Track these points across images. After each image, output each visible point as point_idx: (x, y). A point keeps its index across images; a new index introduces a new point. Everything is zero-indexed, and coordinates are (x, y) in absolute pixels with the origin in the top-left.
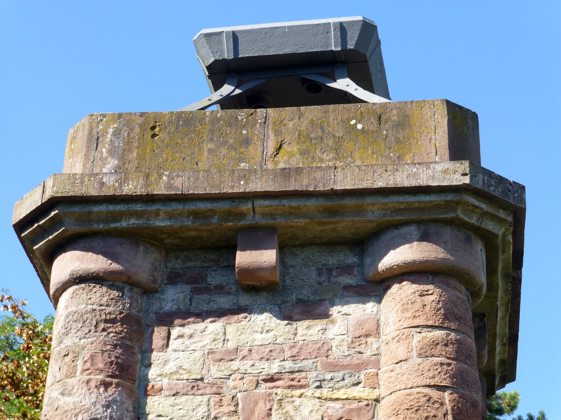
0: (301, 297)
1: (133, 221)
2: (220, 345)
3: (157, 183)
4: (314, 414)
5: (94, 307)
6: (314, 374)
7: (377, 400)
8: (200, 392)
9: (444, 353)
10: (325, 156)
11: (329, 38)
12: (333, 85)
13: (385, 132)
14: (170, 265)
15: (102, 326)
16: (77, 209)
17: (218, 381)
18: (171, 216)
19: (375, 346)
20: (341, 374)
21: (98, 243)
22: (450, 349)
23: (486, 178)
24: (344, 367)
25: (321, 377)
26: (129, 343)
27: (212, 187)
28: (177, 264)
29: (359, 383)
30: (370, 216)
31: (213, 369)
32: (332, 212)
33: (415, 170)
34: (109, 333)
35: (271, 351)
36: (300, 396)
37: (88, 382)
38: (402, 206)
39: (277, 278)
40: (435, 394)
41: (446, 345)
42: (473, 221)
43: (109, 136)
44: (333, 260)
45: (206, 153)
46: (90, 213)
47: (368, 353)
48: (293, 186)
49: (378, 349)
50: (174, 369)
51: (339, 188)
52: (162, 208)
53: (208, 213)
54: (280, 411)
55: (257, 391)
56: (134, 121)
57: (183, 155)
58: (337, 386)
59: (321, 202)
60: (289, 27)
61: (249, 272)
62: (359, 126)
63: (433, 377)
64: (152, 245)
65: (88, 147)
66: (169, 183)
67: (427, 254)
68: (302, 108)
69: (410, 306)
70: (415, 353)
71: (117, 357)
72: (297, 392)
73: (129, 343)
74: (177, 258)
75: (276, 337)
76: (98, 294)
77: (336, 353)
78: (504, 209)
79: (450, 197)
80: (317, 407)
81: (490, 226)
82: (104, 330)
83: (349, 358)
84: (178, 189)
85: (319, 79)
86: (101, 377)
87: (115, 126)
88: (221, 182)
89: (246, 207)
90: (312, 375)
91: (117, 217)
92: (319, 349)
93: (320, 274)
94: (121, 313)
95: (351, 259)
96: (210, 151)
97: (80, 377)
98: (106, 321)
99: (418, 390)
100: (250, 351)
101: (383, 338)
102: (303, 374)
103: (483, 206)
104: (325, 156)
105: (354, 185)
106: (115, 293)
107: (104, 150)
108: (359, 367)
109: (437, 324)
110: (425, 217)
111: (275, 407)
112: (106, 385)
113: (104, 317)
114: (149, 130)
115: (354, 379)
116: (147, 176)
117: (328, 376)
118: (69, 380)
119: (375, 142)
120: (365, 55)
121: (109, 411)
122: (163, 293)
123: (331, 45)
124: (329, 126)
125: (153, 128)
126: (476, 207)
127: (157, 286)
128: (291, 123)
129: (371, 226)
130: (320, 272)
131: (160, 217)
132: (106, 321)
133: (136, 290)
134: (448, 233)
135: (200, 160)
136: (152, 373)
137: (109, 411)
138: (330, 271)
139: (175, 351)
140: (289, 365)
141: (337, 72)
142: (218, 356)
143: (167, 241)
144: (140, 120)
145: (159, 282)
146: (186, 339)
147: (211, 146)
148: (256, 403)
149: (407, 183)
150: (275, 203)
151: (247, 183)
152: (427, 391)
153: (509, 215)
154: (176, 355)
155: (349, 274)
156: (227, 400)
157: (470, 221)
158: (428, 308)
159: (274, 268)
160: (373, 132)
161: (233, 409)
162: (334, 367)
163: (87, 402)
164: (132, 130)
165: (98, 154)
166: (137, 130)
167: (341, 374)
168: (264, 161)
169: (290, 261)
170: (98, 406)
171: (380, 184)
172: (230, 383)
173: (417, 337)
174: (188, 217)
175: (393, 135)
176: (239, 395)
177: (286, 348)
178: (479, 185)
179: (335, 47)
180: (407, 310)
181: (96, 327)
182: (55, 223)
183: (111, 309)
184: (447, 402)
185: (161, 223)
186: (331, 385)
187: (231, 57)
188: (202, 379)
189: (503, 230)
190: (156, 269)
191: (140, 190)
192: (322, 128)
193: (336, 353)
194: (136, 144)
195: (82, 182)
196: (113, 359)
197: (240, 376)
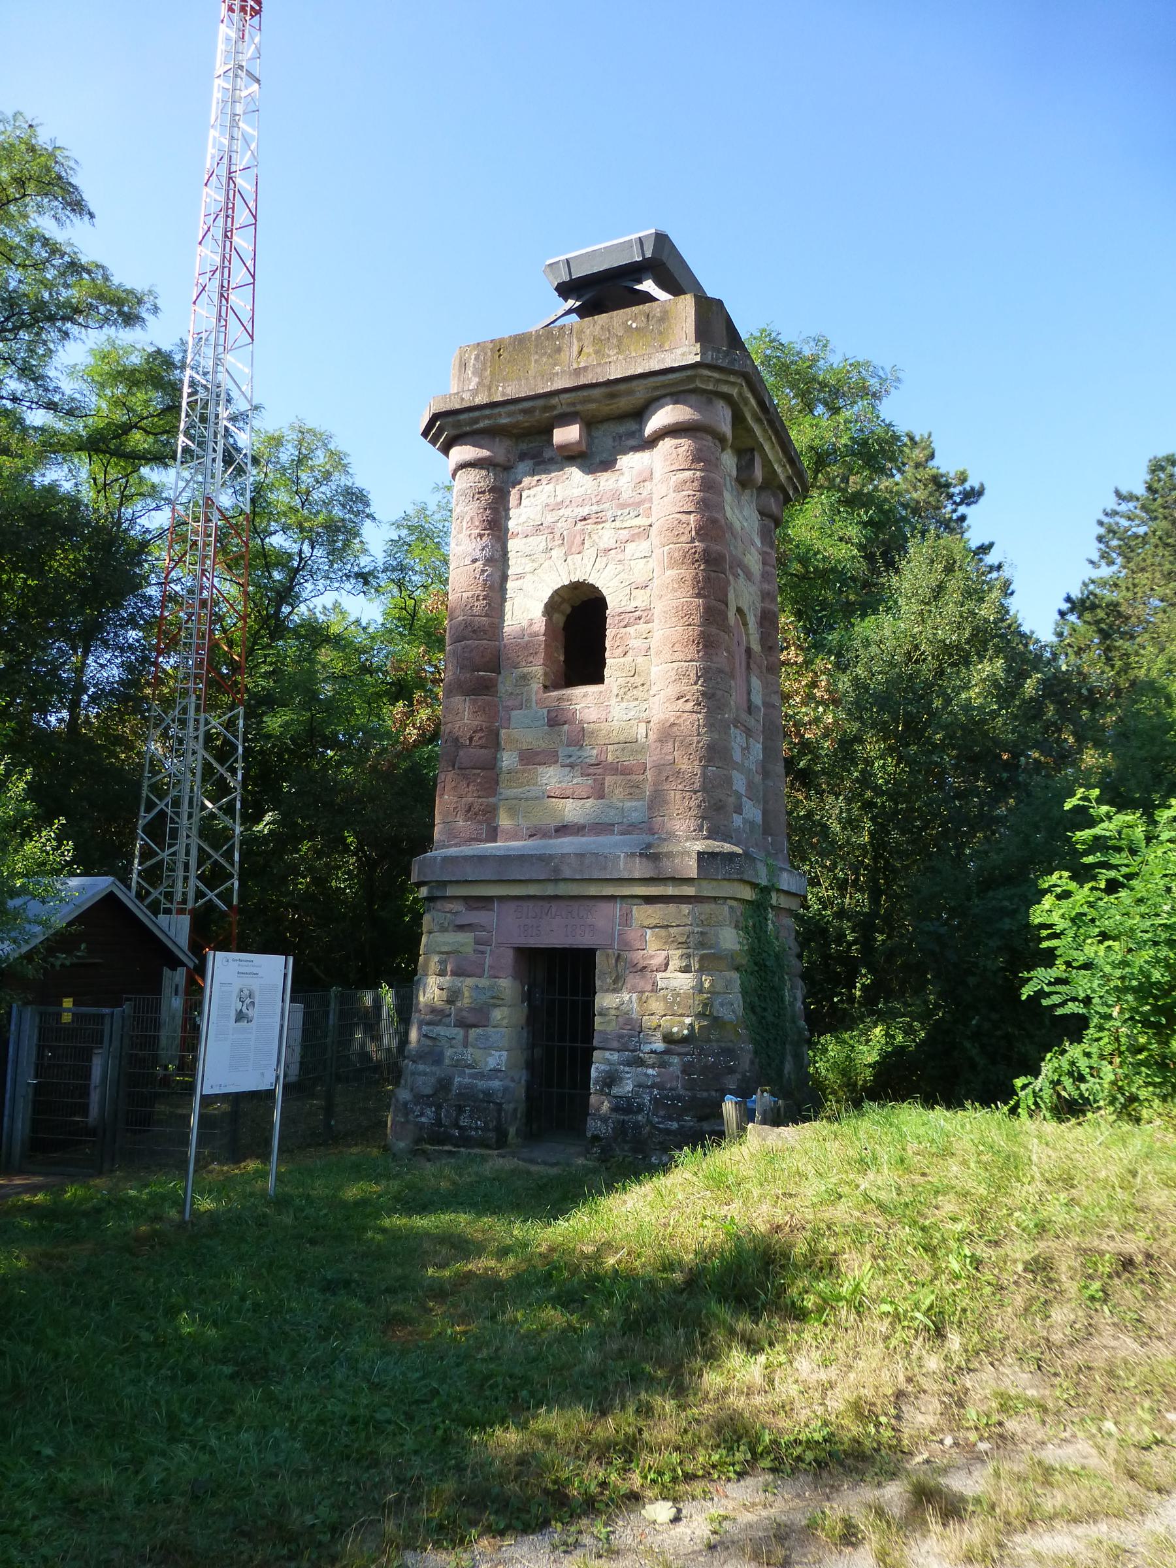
1: (487, 422)
10: (611, 353)
12: (639, 287)
16: (450, 419)
18: (509, 415)
22: (695, 484)
24: (629, 505)
28: (524, 446)
30: (638, 395)
31: (549, 517)
32: (612, 396)
39: (584, 448)
40: (683, 517)
42: (710, 387)
44: (622, 429)
47: (645, 493)
48: (583, 381)
59: (603, 390)
61: (562, 447)
67: (688, 417)
72: (600, 526)
77: (625, 496)
79: (689, 373)
81: (725, 389)
85: (629, 284)
89: (554, 401)
90: (609, 514)
91: (476, 421)
93: (614, 441)
95: (633, 426)
96: (536, 361)
97: (466, 532)
103: (716, 375)
104: (611, 353)
106: (484, 472)
108: (639, 504)
110: (673, 390)
112: (481, 536)
115: (636, 513)
116: (490, 389)
129: (642, 401)
130: (614, 438)
134: (693, 398)
138: (620, 437)
140: (595, 508)
144: (491, 346)
147: (536, 357)
150: (573, 394)
152: (678, 516)
156: (557, 536)
159: (579, 443)
162: (623, 506)
163: (470, 549)
168: (570, 363)
171: (640, 371)
172: (559, 525)
178: (709, 360)
179: (638, 258)
190: (509, 452)
191: (486, 401)
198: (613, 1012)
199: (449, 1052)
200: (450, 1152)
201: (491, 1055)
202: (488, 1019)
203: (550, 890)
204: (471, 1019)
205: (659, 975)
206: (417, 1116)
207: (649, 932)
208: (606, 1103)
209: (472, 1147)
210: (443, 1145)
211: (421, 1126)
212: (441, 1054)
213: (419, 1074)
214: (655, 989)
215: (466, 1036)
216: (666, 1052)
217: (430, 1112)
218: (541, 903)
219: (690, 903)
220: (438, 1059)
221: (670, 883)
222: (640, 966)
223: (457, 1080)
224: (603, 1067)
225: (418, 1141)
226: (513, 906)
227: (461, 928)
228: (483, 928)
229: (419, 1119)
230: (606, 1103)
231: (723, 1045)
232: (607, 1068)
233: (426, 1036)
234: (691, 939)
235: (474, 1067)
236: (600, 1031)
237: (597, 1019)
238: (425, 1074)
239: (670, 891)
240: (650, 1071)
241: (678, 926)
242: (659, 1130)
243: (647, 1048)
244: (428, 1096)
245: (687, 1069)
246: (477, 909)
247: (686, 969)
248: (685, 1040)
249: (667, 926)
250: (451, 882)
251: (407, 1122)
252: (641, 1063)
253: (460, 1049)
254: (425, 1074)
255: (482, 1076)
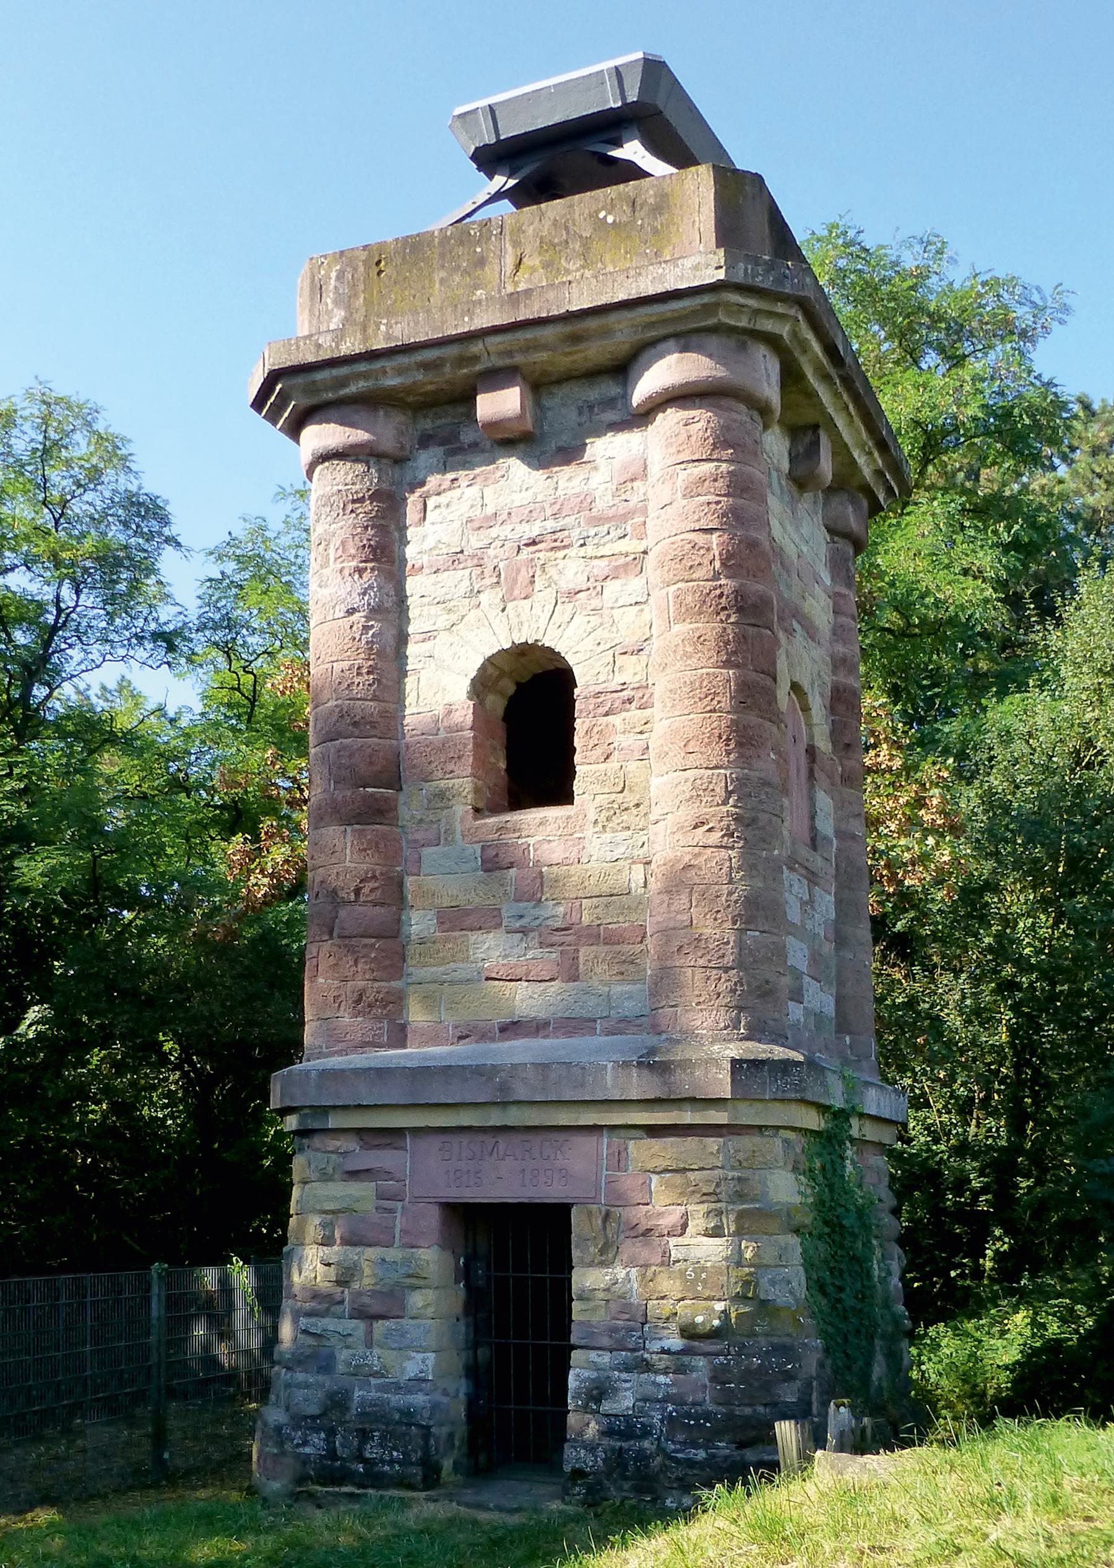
0: (561, 444)
2: (479, 511)
3: (376, 335)
4: (579, 575)
5: (340, 487)
6: (578, 531)
7: (645, 552)
8: (461, 566)
9: (712, 490)
11: (605, 91)
12: (617, 153)
13: (640, 222)
14: (419, 427)
15: (350, 507)
16: (300, 380)
17: (479, 552)
18: (400, 371)
19: (642, 491)
20: (605, 528)
21: (333, 413)
23: (750, 267)
24: (608, 519)
25: (585, 534)
26: (382, 522)
27: (433, 330)
28: (426, 424)
29: (625, 536)
30: (619, 337)
32: (576, 339)
33: (660, 271)
34: (357, 515)
35: (531, 512)
36: (564, 558)
37: (341, 571)
38: (654, 319)
39: (529, 425)
40: (700, 538)
41: (715, 480)
43: (333, 282)
45: (437, 286)
46: (314, 382)
47: (634, 500)
48: (523, 314)
49: (644, 494)
50: (433, 545)
51: (575, 309)
52: (386, 364)
53: (438, 362)
54: (544, 577)
55: (518, 558)
56: (356, 258)
57: (413, 292)
58: (602, 542)
60: (554, 86)
61: (493, 425)
62: (610, 219)
63: (699, 520)
64: (393, 406)
65: (312, 299)
66: (387, 332)
67: (687, 374)
68: (543, 205)
69: (674, 439)
70: (679, 495)
71: (369, 540)
73: (382, 522)
74: (425, 417)
75: (535, 495)
76: (342, 473)
77: (600, 505)
78: (781, 301)
79: (706, 299)
80: (582, 567)
81: (768, 325)
82: (352, 511)
83: (614, 508)
84: (397, 339)
85: (599, 148)
86: (354, 564)
87: (338, 267)
88: (443, 323)
89: (476, 348)
90: (575, 533)
91: (343, 382)
92: (581, 502)
93: (580, 414)
94: (369, 490)
96: (442, 281)
98: (354, 501)
99: (682, 536)
100: (510, 514)
101: (650, 479)
102: (566, 533)
105: (591, 302)
106: (360, 468)
107: (329, 301)
108: (625, 517)
109: (704, 457)
111: (538, 573)
112: (360, 571)
113: (351, 497)
114: (374, 266)
115: (620, 532)
117: (592, 532)
118: (324, 571)
119: (629, 237)
120: (655, 107)
121: (366, 598)
122: (415, 460)
123: (609, 101)
124: (574, 225)
125: (378, 263)
126: (743, 306)
127: (408, 453)
128: (531, 228)
131: (389, 375)
132: (354, 501)
133: (384, 461)
134: (713, 341)
135: (431, 295)
136: (410, 552)
137: (366, 598)
138: (591, 408)
139: (433, 524)
140: (551, 525)
141: (625, 134)
142: (477, 525)
143: (410, 399)
144: (363, 256)
145: (408, 446)
146: (443, 509)
147: (443, 274)
148: (518, 571)
149: (651, 290)
150: (507, 337)
151: (471, 319)
153: (791, 307)
154: (433, 528)
155: (613, 409)
156: (488, 571)
157: (738, 324)
158: (693, 439)
159: (521, 417)
160: (626, 225)
161: (495, 580)
162: (598, 521)
163: (343, 593)
164: (355, 269)
165: (322, 307)
166: (361, 269)
167: (605, 528)
168: (502, 284)
169: (547, 402)
170: (355, 595)
171: (622, 296)
172: (491, 552)
173: (683, 475)
174: (418, 370)
175: (649, 224)
176: (501, 565)
177: (547, 506)
178: (739, 277)
180: (671, 444)
181: (344, 509)
182: (283, 398)
183: (358, 487)
184: (715, 546)
185: (392, 381)
186: (596, 541)
187: (494, 141)
188: (462, 552)
189: (787, 328)
192: (567, 228)
193: (600, 505)
194: (362, 287)
195: (298, 347)
196: (365, 542)
197: (501, 543)
198: (601, 1295)
199: (343, 1355)
200: (351, 1495)
201: (409, 1358)
202: (403, 1306)
203: (495, 1118)
204: (375, 1308)
205: (673, 1241)
206: (298, 1446)
207: (655, 1178)
208: (593, 1424)
209: (386, 1487)
210: (340, 1485)
211: (305, 1460)
212: (332, 1357)
213: (299, 1386)
214: (667, 1261)
215: (370, 1332)
216: (684, 1352)
217: (318, 1440)
218: (481, 1137)
219: (721, 1136)
220: (326, 1365)
221: (687, 1106)
222: (642, 1228)
223: (357, 1394)
224: (587, 1374)
225: (301, 1480)
226: (436, 1142)
227: (354, 1175)
228: (388, 1175)
229: (301, 1450)
230: (593, 1424)
231: (775, 1340)
232: (594, 1375)
233: (305, 1332)
234: (723, 1188)
235: (383, 1376)
236: (581, 1323)
237: (576, 1306)
238: (308, 1386)
239: (688, 1117)
240: (661, 1379)
241: (702, 1169)
242: (677, 1461)
243: (655, 1346)
244: (313, 1418)
245: (718, 1376)
246: (377, 1147)
247: (715, 1232)
248: (714, 1334)
249: (685, 1170)
250: (335, 1107)
251: (283, 1453)
252: (646, 1367)
253: (361, 1350)
254: (308, 1386)
255: (398, 1388)
